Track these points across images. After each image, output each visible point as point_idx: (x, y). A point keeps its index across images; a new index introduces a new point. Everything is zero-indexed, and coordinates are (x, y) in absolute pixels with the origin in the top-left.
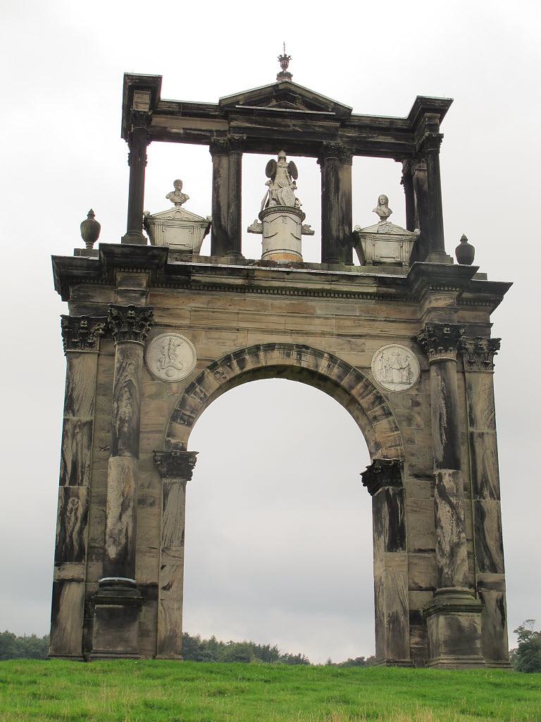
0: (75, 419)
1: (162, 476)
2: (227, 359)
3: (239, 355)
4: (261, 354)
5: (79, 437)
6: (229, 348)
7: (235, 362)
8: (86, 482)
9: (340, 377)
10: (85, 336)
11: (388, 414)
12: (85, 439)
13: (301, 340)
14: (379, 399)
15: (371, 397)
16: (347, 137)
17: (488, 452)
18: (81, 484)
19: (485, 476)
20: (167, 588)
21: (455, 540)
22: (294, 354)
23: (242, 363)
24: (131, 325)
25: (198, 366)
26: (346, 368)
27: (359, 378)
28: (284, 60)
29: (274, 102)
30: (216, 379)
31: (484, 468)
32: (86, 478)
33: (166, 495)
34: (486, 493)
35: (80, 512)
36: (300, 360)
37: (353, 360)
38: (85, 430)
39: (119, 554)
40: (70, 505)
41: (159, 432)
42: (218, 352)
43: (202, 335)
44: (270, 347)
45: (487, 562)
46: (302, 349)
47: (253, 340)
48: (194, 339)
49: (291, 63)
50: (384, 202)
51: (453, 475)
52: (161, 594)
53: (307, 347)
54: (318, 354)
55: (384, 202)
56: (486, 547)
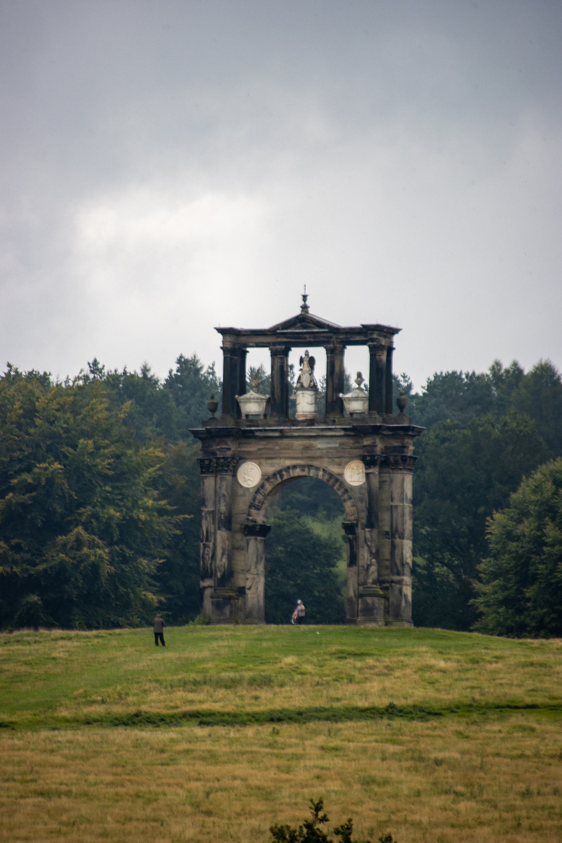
0: (206, 510)
1: (246, 535)
2: (274, 475)
3: (280, 472)
4: (291, 471)
5: (208, 519)
6: (277, 468)
7: (278, 476)
8: (212, 541)
9: (328, 480)
10: (209, 467)
11: (350, 498)
12: (211, 519)
13: (310, 463)
14: (346, 491)
15: (343, 490)
16: (340, 339)
17: (399, 515)
18: (210, 542)
19: (397, 527)
20: (249, 589)
21: (369, 563)
22: (306, 469)
23: (282, 476)
24: (223, 466)
25: (262, 479)
26: (331, 475)
27: (337, 480)
28: (305, 297)
29: (299, 325)
30: (270, 485)
31: (397, 523)
32: (212, 538)
33: (248, 545)
34: (397, 536)
35: (211, 554)
36: (309, 472)
37: (335, 470)
38: (211, 515)
39: (221, 576)
40: (206, 552)
41: (245, 513)
42: (271, 470)
43: (263, 461)
44: (295, 467)
45: (395, 570)
46: (310, 467)
47: (288, 463)
48: (260, 465)
49: (308, 298)
50: (359, 375)
51: (370, 532)
52: (248, 592)
53: (312, 466)
54: (317, 469)
55: (359, 375)
56: (396, 564)
